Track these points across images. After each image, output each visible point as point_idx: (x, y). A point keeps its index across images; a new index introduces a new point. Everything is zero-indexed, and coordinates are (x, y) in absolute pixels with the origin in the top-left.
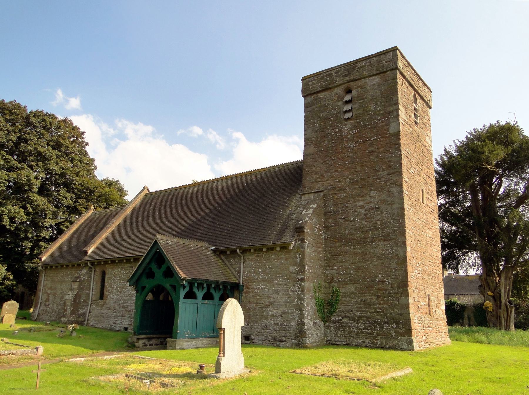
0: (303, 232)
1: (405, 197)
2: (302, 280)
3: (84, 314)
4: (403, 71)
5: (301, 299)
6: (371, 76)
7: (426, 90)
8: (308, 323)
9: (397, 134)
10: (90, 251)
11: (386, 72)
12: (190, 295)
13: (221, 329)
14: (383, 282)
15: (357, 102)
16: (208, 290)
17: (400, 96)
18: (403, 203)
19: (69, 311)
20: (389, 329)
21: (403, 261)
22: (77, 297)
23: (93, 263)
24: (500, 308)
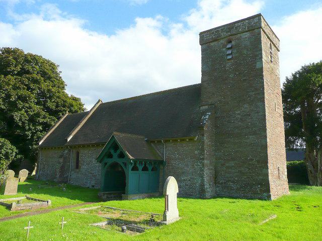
0: (203, 130)
1: (266, 108)
2: (203, 159)
3: (68, 176)
4: (264, 29)
5: (203, 170)
6: (244, 32)
7: (277, 40)
8: (207, 186)
9: (261, 69)
10: (69, 140)
11: (254, 30)
12: (135, 169)
13: (166, 195)
14: (252, 160)
15: (235, 50)
16: (145, 165)
17: (263, 45)
18: (265, 112)
19: (58, 176)
20: (257, 188)
21: (265, 147)
22: (62, 167)
23: (71, 147)
24: (317, 172)
